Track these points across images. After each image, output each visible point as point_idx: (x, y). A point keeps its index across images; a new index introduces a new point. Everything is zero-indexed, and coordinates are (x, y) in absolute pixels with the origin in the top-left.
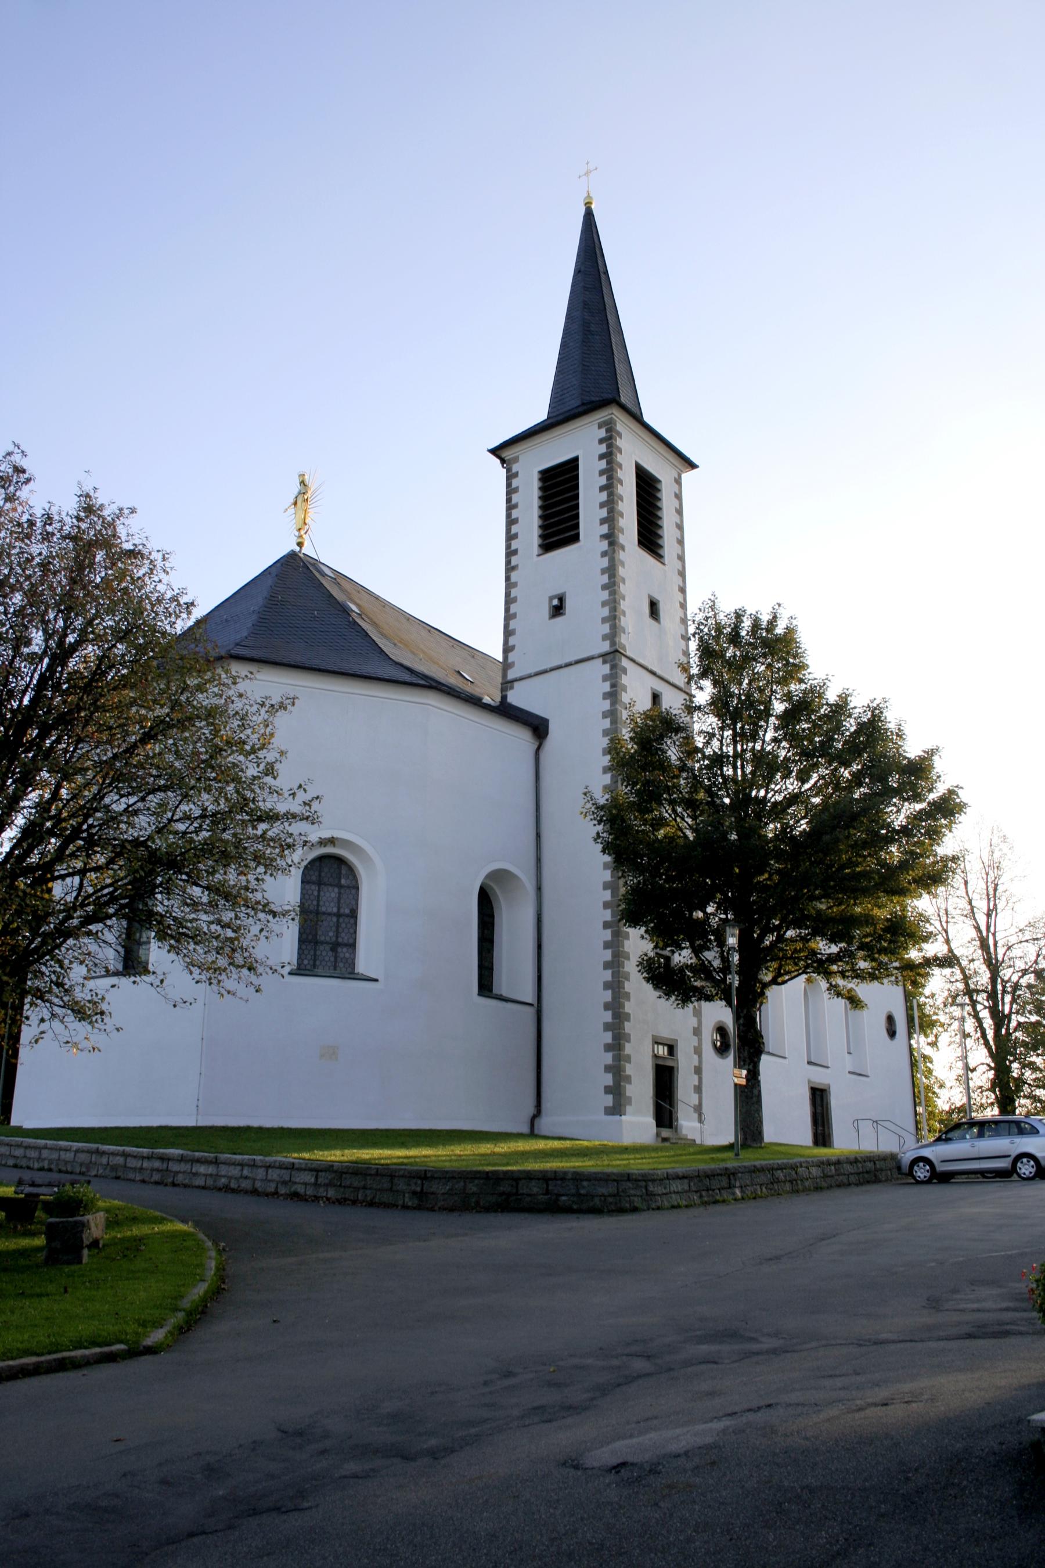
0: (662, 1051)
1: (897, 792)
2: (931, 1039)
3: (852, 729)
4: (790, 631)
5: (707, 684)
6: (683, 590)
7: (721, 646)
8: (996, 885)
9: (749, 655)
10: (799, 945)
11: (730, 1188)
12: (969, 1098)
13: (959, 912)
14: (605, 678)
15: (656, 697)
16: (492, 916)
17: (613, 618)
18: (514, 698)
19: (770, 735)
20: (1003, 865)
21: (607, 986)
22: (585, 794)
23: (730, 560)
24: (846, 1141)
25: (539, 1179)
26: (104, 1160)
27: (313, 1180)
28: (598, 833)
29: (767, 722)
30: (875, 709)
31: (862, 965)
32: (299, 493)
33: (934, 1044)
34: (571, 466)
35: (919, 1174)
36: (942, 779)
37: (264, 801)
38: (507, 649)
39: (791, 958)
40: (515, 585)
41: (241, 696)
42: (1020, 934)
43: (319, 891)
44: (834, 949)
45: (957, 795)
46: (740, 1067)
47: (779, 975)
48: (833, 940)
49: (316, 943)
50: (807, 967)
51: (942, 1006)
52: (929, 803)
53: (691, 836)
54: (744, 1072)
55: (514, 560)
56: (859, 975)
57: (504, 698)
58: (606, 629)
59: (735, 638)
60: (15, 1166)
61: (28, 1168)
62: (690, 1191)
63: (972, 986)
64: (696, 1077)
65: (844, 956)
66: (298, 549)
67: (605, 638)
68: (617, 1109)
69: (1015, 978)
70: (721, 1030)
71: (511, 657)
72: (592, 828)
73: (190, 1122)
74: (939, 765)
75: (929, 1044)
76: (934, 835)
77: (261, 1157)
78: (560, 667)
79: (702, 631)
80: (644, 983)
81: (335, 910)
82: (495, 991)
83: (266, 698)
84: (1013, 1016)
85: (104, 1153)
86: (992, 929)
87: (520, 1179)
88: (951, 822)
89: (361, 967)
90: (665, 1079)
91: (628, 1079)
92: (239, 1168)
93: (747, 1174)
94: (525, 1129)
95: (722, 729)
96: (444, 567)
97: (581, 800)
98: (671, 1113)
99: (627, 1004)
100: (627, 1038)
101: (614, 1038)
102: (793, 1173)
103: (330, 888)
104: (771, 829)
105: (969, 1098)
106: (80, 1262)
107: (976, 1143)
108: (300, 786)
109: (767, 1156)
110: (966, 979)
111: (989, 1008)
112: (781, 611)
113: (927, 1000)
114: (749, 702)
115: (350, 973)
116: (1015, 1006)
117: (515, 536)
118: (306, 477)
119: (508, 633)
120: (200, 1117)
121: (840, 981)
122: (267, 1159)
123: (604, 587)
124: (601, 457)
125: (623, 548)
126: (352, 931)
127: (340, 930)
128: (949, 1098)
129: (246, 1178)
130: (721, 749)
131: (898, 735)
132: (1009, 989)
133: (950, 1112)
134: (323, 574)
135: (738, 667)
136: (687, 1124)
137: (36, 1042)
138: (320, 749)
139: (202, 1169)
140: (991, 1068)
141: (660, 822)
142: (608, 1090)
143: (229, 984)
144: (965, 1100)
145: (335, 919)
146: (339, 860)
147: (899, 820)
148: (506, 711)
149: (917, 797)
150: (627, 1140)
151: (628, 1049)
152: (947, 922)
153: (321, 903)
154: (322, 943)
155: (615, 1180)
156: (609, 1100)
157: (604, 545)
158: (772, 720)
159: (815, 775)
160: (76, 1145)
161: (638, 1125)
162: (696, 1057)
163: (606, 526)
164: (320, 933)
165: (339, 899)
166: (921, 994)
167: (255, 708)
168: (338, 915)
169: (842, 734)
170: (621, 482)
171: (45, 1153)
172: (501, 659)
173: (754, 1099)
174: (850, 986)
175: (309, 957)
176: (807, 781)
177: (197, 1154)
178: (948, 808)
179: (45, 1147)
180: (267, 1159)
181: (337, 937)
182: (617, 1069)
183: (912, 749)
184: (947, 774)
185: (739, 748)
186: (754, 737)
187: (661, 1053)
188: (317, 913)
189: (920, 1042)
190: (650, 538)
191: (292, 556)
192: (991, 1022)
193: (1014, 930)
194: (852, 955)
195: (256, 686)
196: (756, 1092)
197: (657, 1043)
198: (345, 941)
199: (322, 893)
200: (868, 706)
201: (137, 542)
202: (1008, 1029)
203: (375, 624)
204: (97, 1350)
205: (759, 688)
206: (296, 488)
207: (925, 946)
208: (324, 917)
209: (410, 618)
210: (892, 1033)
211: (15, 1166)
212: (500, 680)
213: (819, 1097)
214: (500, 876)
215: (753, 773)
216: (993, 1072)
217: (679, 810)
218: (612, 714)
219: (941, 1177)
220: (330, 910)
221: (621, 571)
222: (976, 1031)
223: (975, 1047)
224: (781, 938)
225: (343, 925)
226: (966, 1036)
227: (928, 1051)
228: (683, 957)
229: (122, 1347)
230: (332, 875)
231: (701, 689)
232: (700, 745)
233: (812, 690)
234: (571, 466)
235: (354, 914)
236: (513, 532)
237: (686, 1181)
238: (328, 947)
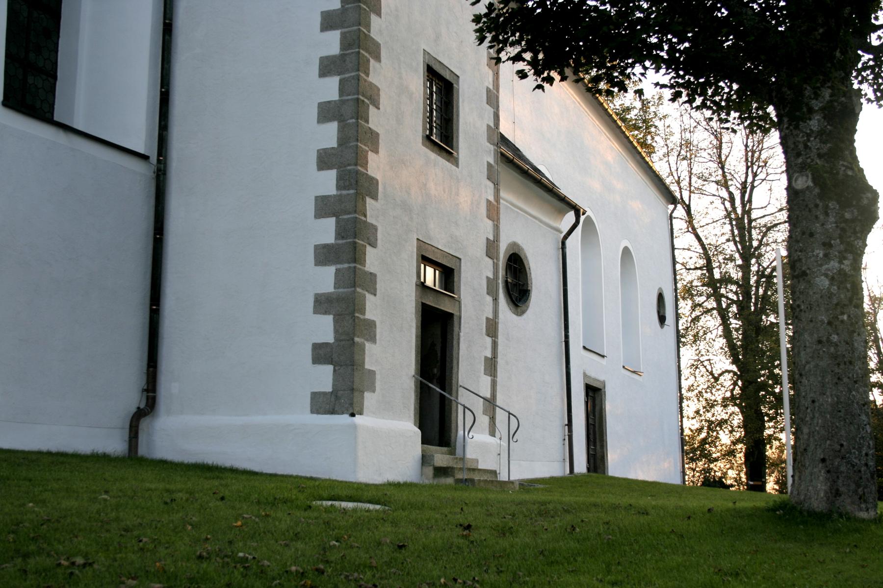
0: (430, 276)
68: (343, 399)
90: (437, 331)
101: (340, 233)
136: (479, 445)
142: (321, 354)
151: (373, 260)
156: (324, 378)
161: (382, 444)
182: (346, 307)
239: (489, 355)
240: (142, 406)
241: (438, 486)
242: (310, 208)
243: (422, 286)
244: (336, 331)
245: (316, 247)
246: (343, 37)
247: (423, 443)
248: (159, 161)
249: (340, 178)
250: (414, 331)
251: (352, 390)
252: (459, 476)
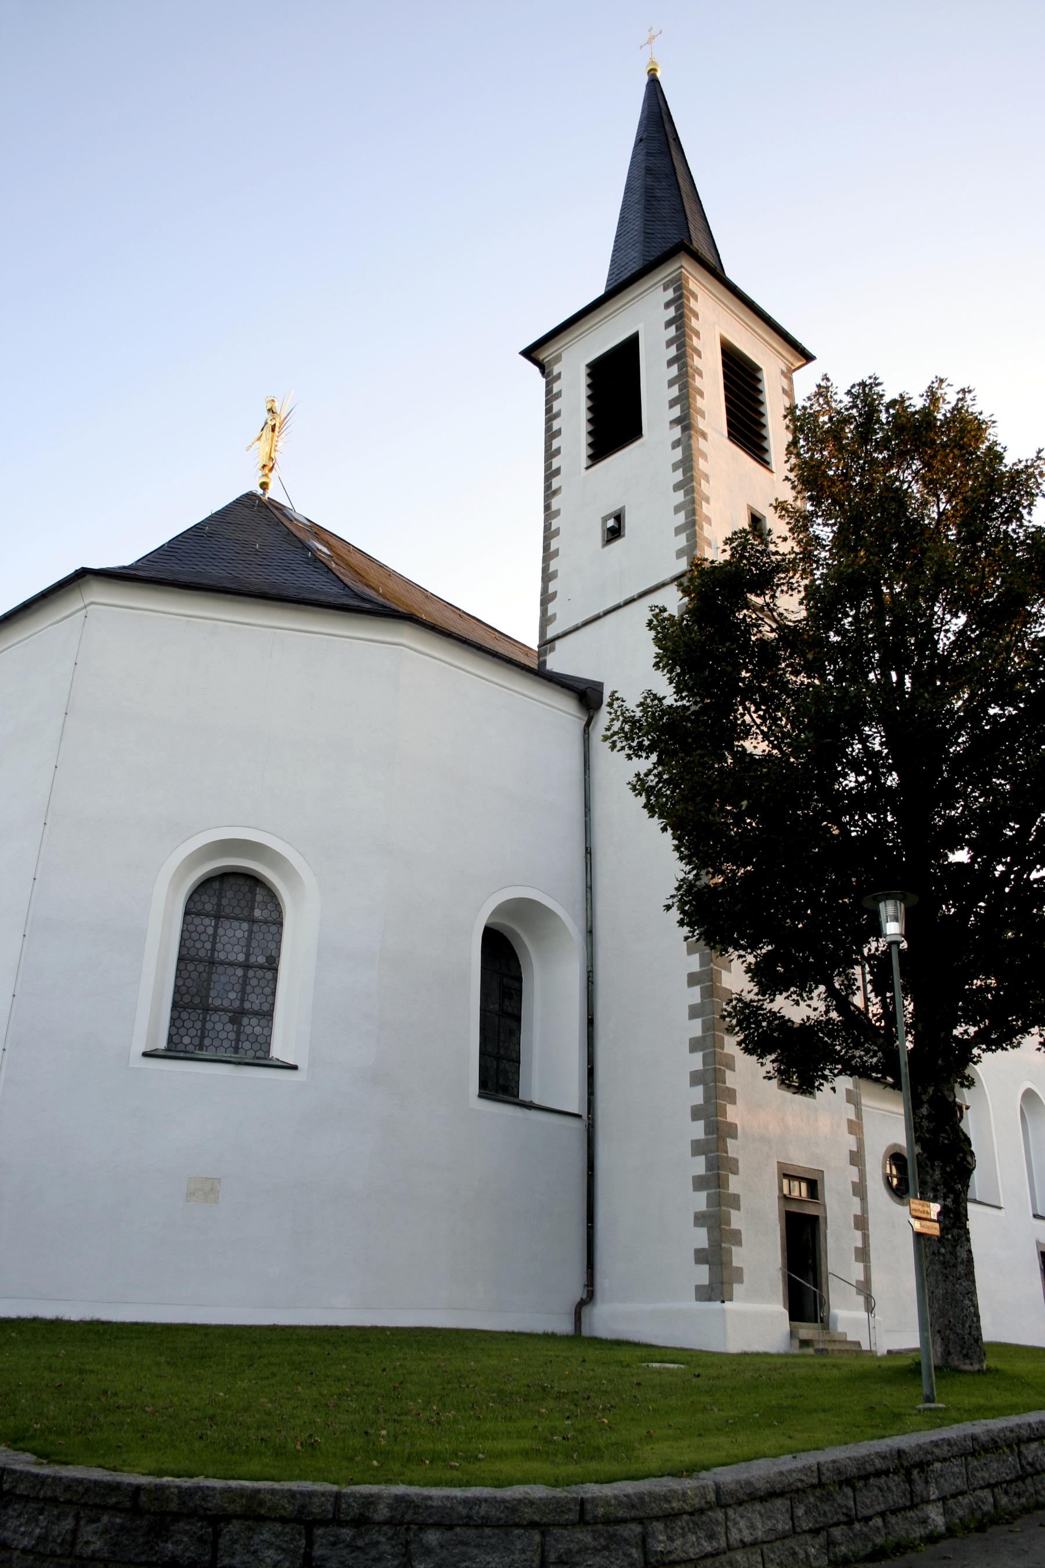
0: (800, 1190)
11: (913, 1506)
21: (696, 1079)
25: (284, 1520)
34: (631, 345)
43: (216, 928)
49: (206, 1009)
54: (935, 1208)
62: (794, 1532)
66: (260, 491)
68: (718, 1287)
78: (618, 607)
81: (241, 958)
82: (523, 1096)
87: (227, 1518)
89: (277, 1052)
90: (803, 1239)
91: (736, 1237)
98: (821, 1296)
99: (730, 1108)
101: (709, 1167)
103: (236, 924)
115: (262, 1060)
126: (267, 990)
127: (249, 989)
136: (846, 1314)
142: (701, 1256)
145: (240, 972)
146: (253, 881)
151: (735, 1184)
153: (219, 946)
154: (216, 1010)
155: (533, 1525)
156: (702, 1274)
157: (677, 432)
161: (755, 1320)
162: (856, 1200)
164: (213, 993)
165: (249, 940)
168: (246, 966)
173: (961, 1269)
175: (192, 1032)
181: (242, 1001)
182: (717, 1222)
187: (795, 1194)
188: (212, 962)
191: (249, 498)
196: (962, 1254)
197: (786, 1176)
198: (256, 1007)
199: (221, 931)
208: (221, 969)
214: (524, 910)
220: (232, 957)
221: (701, 464)
225: (254, 982)
234: (631, 345)
235: (272, 965)
237: (779, 1503)
238: (225, 1018)
239: (860, 1245)
240: (584, 1297)
241: (804, 1356)
242: (688, 1149)
244: (709, 1239)
245: (694, 1178)
246: (704, 1022)
247: (791, 1319)
248: (589, 1118)
249: (706, 1126)
250: (779, 1234)
251: (722, 1283)
252: (821, 1346)
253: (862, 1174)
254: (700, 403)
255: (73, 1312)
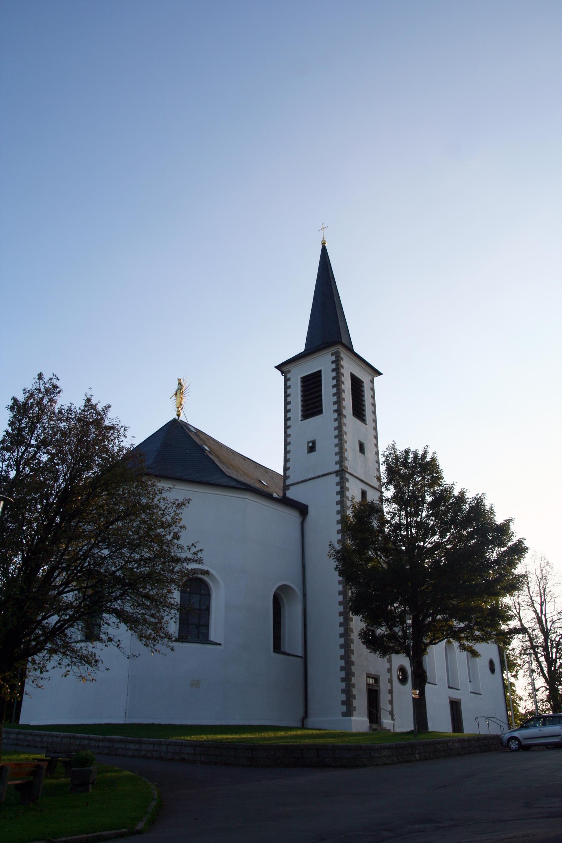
0: (371, 681)
1: (492, 542)
2: (514, 673)
3: (467, 510)
4: (434, 460)
5: (391, 487)
6: (376, 437)
7: (398, 468)
8: (545, 589)
9: (415, 472)
10: (444, 623)
12: (537, 706)
13: (525, 603)
14: (337, 484)
15: (364, 494)
16: (280, 610)
17: (341, 453)
18: (290, 494)
19: (424, 514)
20: (548, 577)
21: (342, 646)
22: (330, 545)
23: (401, 423)
24: (470, 728)
26: (78, 742)
27: (193, 751)
28: (337, 566)
29: (423, 506)
30: (479, 499)
31: (477, 633)
32: (178, 389)
33: (515, 676)
34: (318, 374)
35: (512, 746)
36: (515, 534)
37: (174, 552)
38: (286, 469)
39: (439, 630)
40: (289, 436)
41: (164, 499)
42: (559, 615)
43: (190, 597)
44: (462, 625)
45: (523, 543)
46: (416, 689)
47: (434, 639)
48: (461, 621)
50: (448, 634)
51: (518, 655)
52: (508, 547)
53: (385, 565)
54: (418, 692)
55: (289, 423)
56: (477, 639)
57: (284, 494)
58: (337, 458)
59: (405, 463)
60: (28, 746)
61: (35, 746)
63: (535, 644)
64: (390, 695)
65: (467, 629)
67: (337, 463)
68: (349, 713)
69: (557, 639)
70: (402, 669)
71: (288, 473)
72: (333, 563)
73: (122, 722)
74: (513, 527)
75: (513, 676)
76: (512, 564)
77: (164, 740)
79: (388, 460)
80: (362, 644)
81: (198, 607)
82: (282, 650)
83: (176, 500)
84: (558, 660)
85: (78, 738)
86: (544, 613)
88: (520, 557)
89: (212, 638)
90: (373, 696)
92: (152, 745)
93: (420, 746)
94: (299, 725)
95: (400, 510)
96: (253, 427)
97: (328, 549)
99: (352, 656)
100: (353, 674)
102: (446, 746)
104: (427, 563)
105: (537, 706)
106: (88, 791)
107: (542, 729)
108: (193, 545)
109: (431, 737)
110: (531, 640)
111: (544, 655)
112: (428, 449)
113: (510, 652)
114: (414, 497)
116: (558, 654)
117: (289, 411)
118: (182, 381)
119: (286, 460)
120: (127, 719)
121: (466, 643)
122: (167, 740)
123: (336, 437)
124: (333, 370)
125: (345, 417)
128: (525, 706)
129: (156, 751)
130: (400, 521)
131: (491, 512)
132: (555, 645)
133: (525, 715)
134: (191, 431)
135: (407, 479)
136: (386, 722)
137: (65, 676)
138: (203, 524)
139: (132, 746)
140: (547, 689)
141: (370, 559)
142: (343, 703)
143: (158, 647)
144: (534, 708)
146: (202, 581)
147: (493, 556)
148: (285, 501)
149: (502, 545)
150: (354, 730)
151: (354, 680)
152: (519, 609)
156: (344, 708)
157: (336, 415)
158: (426, 505)
159: (449, 534)
160: (62, 734)
161: (359, 722)
162: (389, 684)
163: (336, 406)
166: (507, 649)
167: (170, 505)
169: (462, 513)
170: (343, 383)
171: (45, 739)
172: (282, 474)
174: (471, 644)
176: (444, 538)
177: (129, 738)
178: (519, 550)
179: (45, 735)
180: (167, 740)
182: (348, 692)
183: (499, 520)
184: (518, 532)
185: (409, 520)
186: (417, 515)
189: (507, 675)
190: (359, 412)
192: (545, 663)
193: (555, 613)
194: (471, 628)
195: (170, 493)
200: (475, 498)
201: (114, 423)
202: (555, 667)
203: (217, 457)
204: (115, 831)
205: (418, 489)
206: (176, 386)
207: (509, 622)
209: (234, 453)
210: (493, 670)
211: (28, 746)
212: (282, 484)
213: (455, 706)
215: (416, 533)
216: (548, 691)
217: (379, 553)
218: (341, 503)
219: (524, 748)
222: (538, 668)
223: (538, 678)
224: (434, 619)
226: (533, 671)
227: (512, 680)
228: (381, 631)
229: (126, 830)
230: (197, 588)
231: (389, 490)
232: (389, 519)
233: (446, 489)
234: (318, 374)
236: (288, 408)
242: (339, 669)
243: (368, 684)
253: (391, 676)
254: (344, 403)
255: (163, 722)
